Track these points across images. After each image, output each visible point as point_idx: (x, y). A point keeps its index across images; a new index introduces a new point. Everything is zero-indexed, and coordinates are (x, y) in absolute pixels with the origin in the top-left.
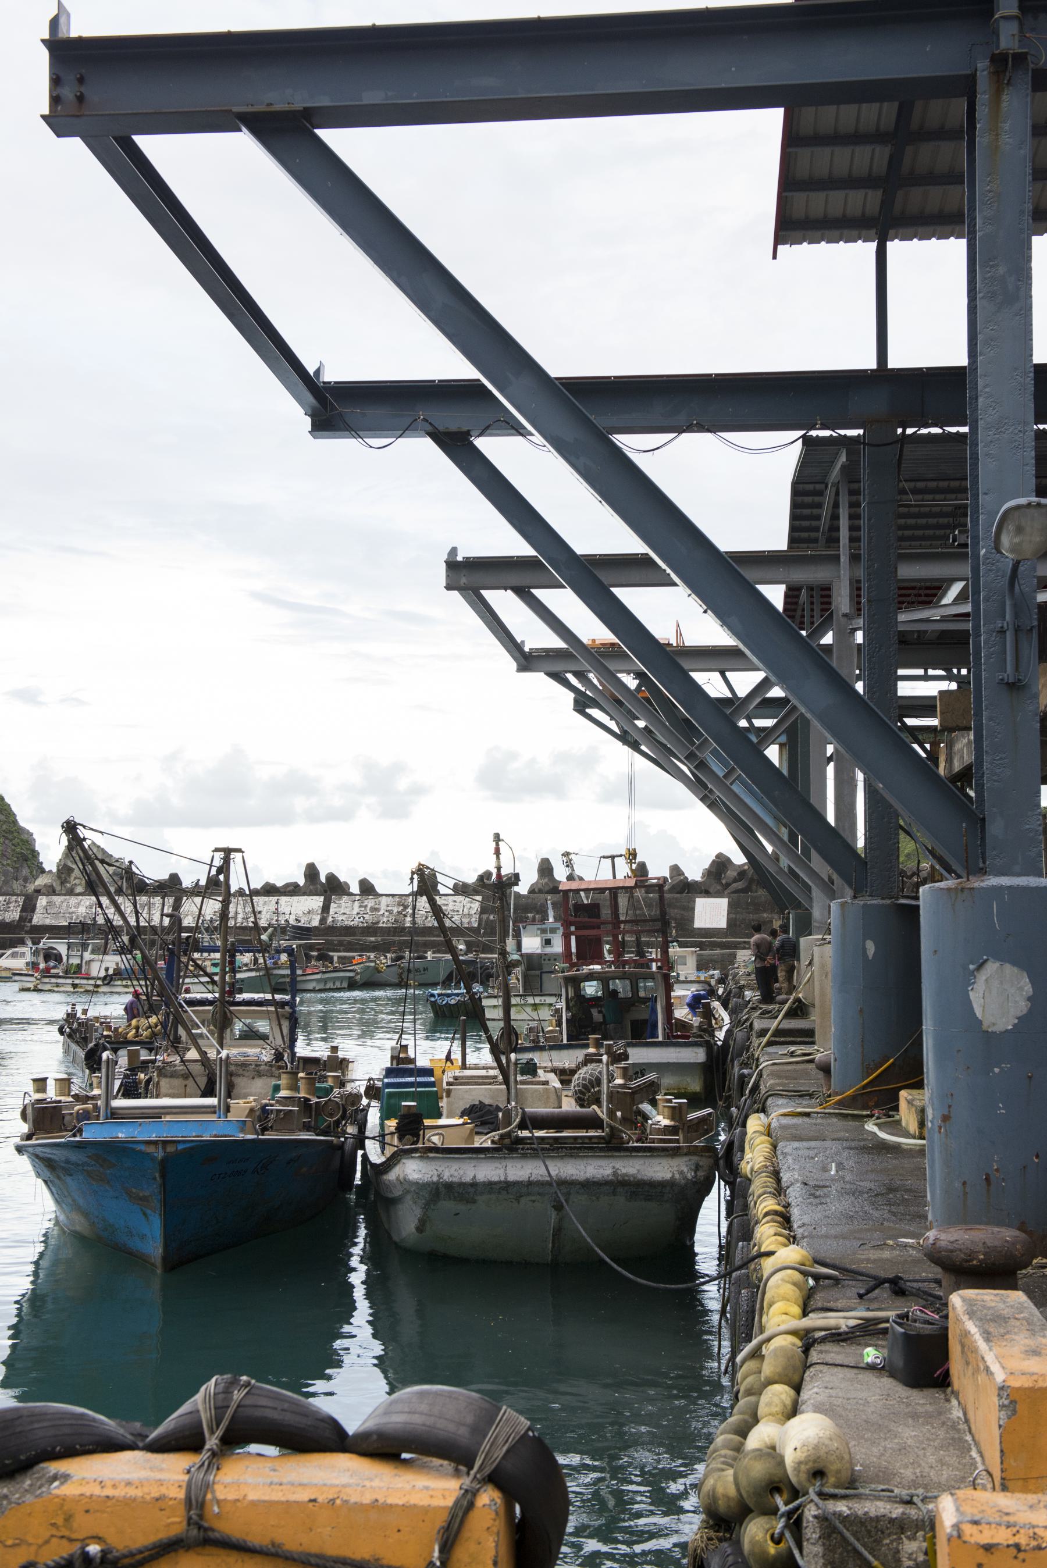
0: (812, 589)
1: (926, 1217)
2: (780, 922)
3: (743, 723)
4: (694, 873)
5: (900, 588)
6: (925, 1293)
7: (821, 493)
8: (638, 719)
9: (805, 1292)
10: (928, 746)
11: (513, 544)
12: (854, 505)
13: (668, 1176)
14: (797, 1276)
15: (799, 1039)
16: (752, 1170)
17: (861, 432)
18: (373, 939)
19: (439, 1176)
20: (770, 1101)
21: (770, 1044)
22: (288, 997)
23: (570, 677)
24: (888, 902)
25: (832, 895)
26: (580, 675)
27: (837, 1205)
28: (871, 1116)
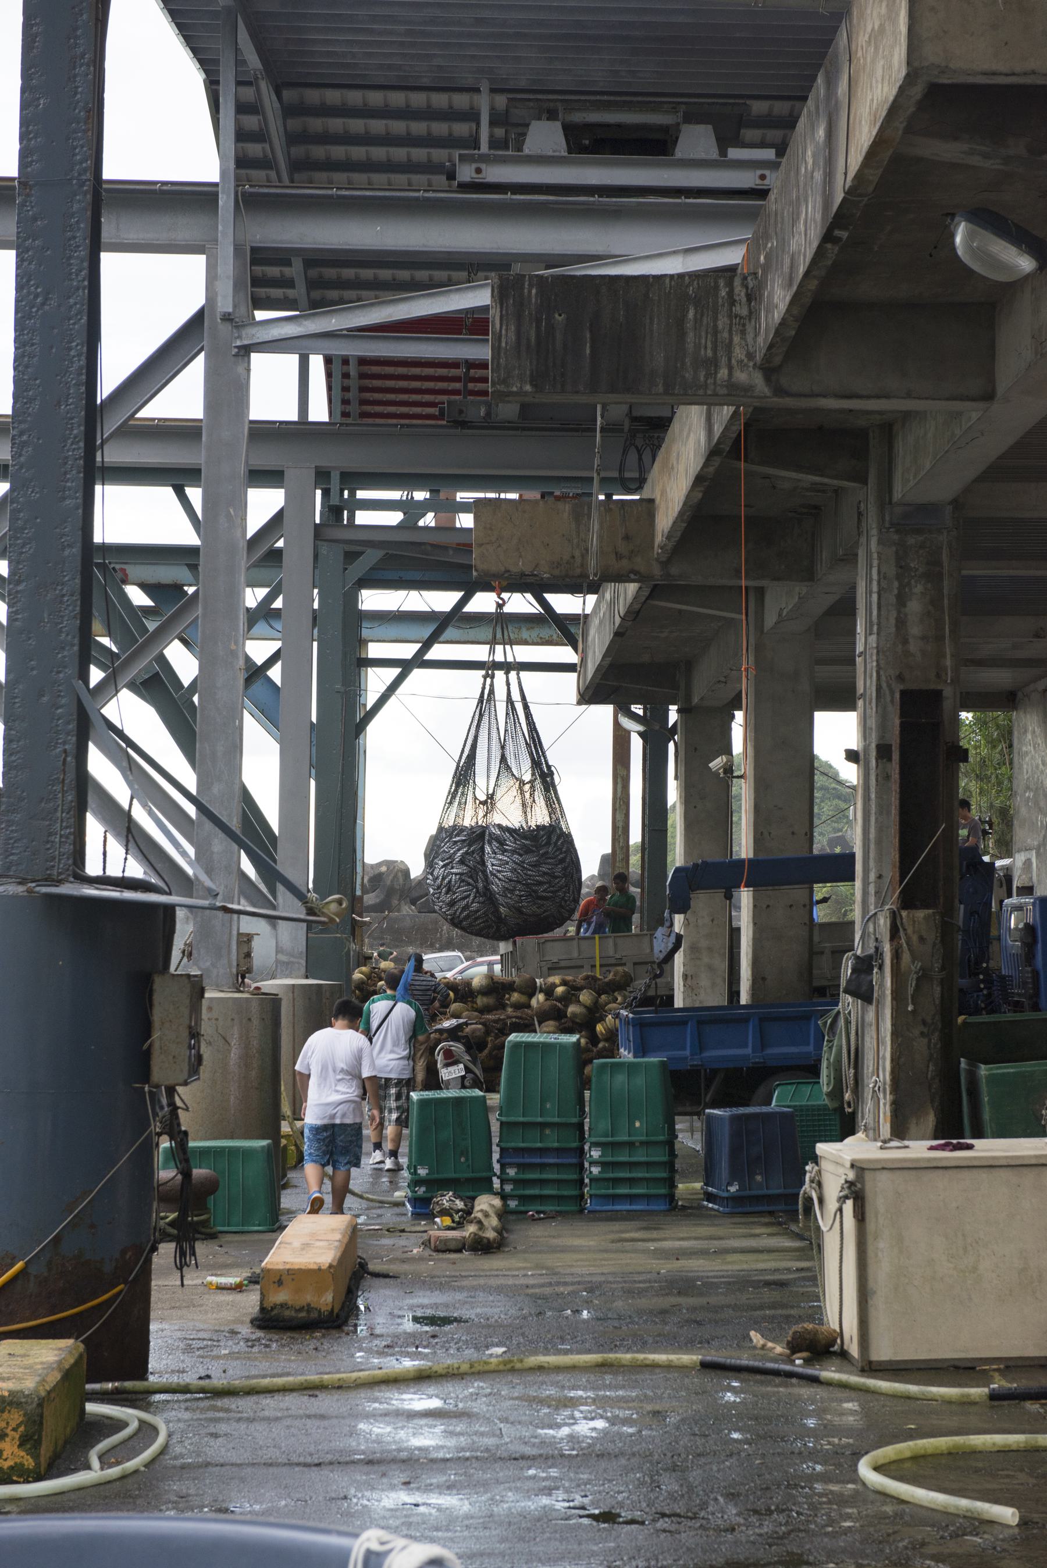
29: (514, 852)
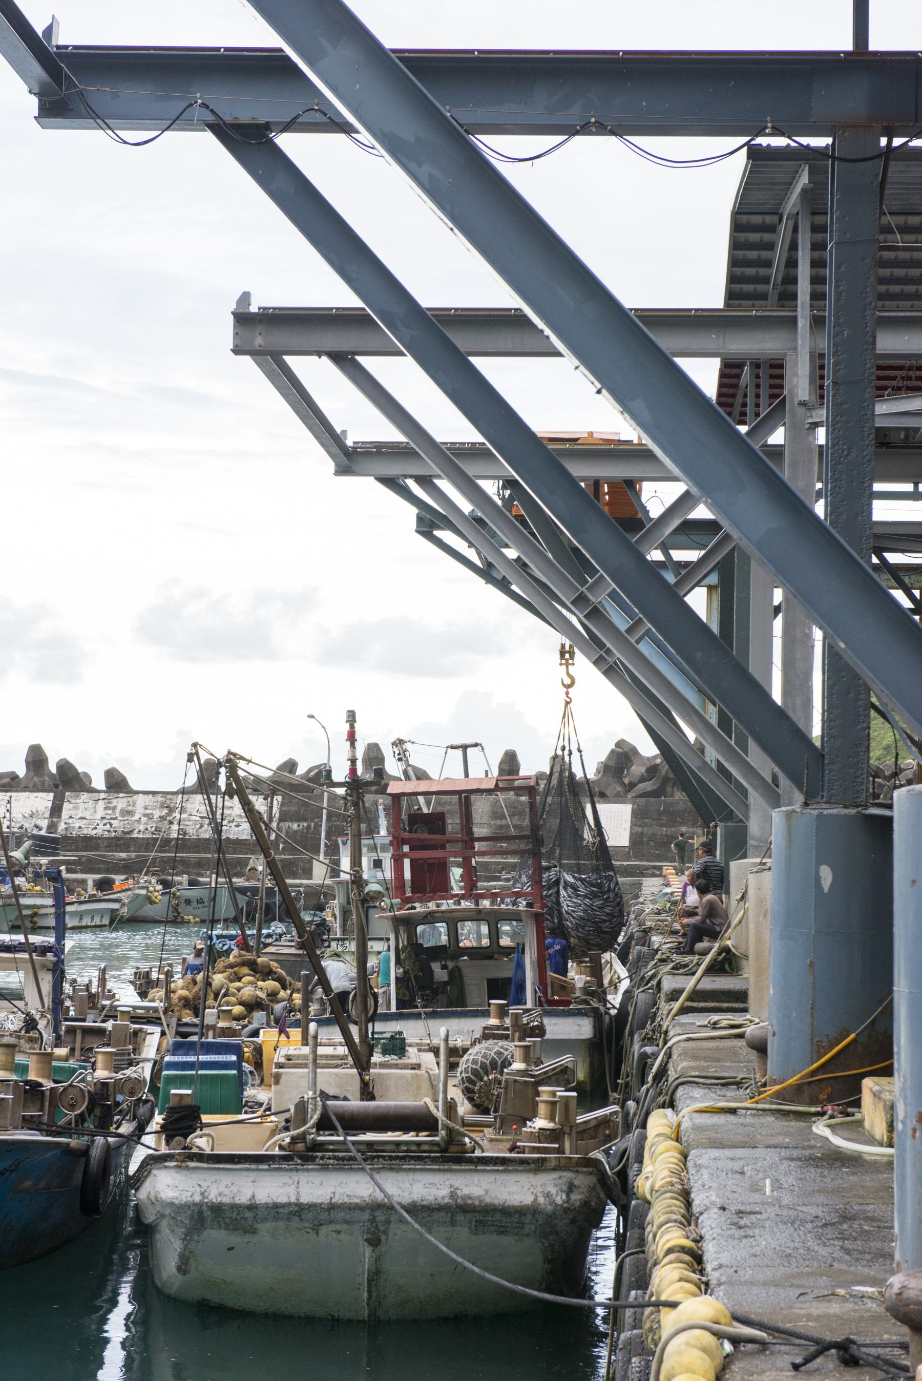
0: (758, 366)
1: (891, 1256)
2: (703, 839)
3: (656, 555)
4: (588, 766)
5: (879, 368)
6: (887, 1362)
7: (772, 229)
8: (507, 546)
9: (719, 1361)
10: (917, 593)
11: (332, 291)
12: (818, 246)
13: (528, 1200)
14: (708, 1339)
15: (725, 1005)
16: (652, 1190)
17: (829, 140)
18: (123, 855)
19: (202, 1194)
20: (680, 1092)
21: (684, 1011)
22: (52, 940)
23: (411, 484)
24: (853, 811)
25: (775, 800)
26: (425, 481)
27: (771, 1239)
28: (822, 1114)
29: (585, 896)
